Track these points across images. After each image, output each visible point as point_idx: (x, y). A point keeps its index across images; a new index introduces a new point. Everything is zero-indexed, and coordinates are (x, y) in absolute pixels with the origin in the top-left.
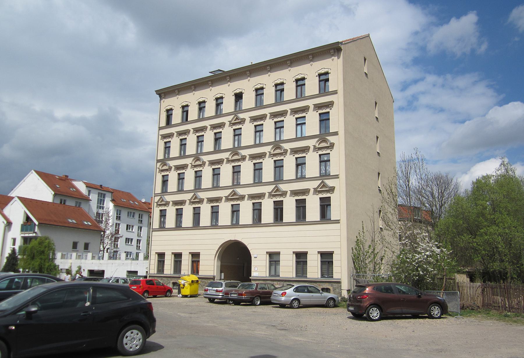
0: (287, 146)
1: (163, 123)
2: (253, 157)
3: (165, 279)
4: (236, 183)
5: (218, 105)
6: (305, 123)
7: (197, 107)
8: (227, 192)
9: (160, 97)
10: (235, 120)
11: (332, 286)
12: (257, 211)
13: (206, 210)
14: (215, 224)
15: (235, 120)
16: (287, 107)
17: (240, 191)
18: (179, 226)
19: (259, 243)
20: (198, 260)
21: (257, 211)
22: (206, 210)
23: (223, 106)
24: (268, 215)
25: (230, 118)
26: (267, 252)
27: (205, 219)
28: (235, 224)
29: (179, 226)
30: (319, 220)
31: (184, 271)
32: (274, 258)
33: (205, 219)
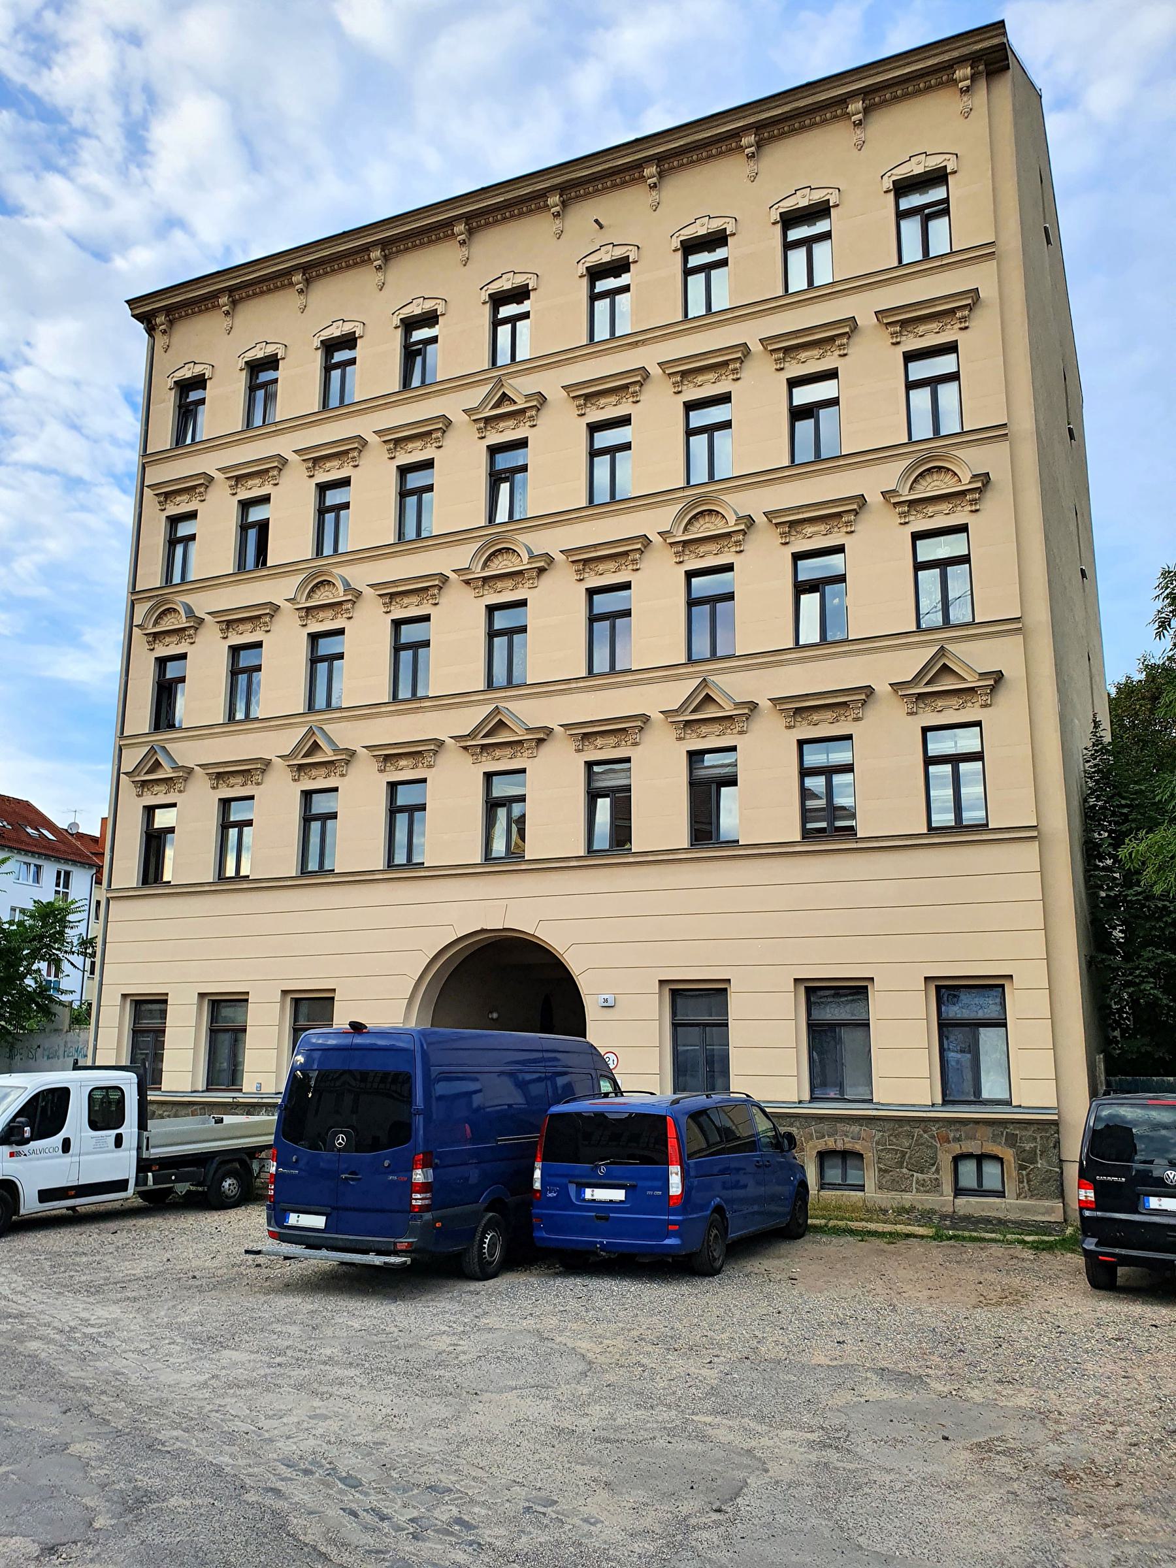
0: (362, 576)
1: (163, 438)
2: (585, 560)
3: (855, 1129)
4: (502, 679)
5: (412, 354)
6: (524, 468)
7: (241, 381)
8: (469, 719)
9: (151, 330)
10: (497, 405)
11: (1012, 1141)
12: (609, 792)
13: (360, 801)
14: (401, 864)
15: (497, 405)
16: (365, 426)
17: (528, 712)
18: (313, 870)
19: (619, 949)
20: (859, 1016)
21: (609, 792)
22: (360, 801)
23: (204, 416)
24: (662, 816)
25: (475, 396)
26: (202, 995)
27: (358, 836)
28: (507, 855)
29: (827, 826)
30: (685, 844)
31: (260, 1078)
32: (697, 1010)
33: (358, 836)
